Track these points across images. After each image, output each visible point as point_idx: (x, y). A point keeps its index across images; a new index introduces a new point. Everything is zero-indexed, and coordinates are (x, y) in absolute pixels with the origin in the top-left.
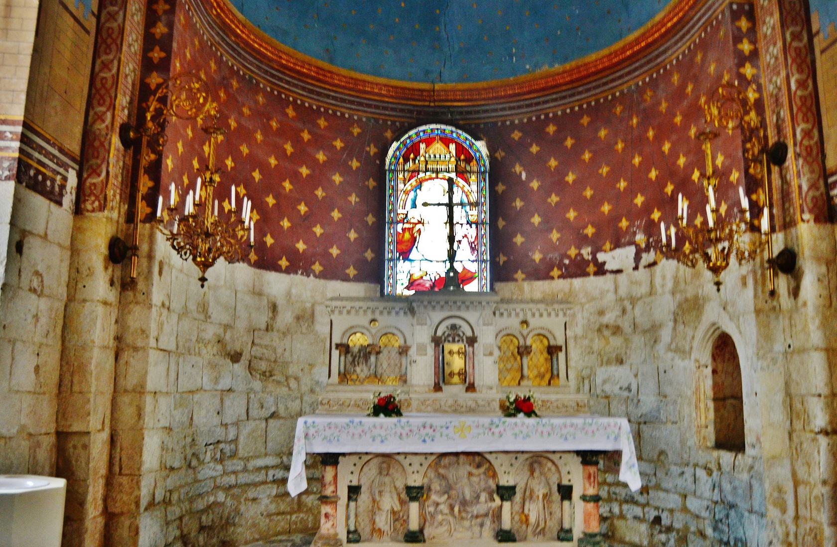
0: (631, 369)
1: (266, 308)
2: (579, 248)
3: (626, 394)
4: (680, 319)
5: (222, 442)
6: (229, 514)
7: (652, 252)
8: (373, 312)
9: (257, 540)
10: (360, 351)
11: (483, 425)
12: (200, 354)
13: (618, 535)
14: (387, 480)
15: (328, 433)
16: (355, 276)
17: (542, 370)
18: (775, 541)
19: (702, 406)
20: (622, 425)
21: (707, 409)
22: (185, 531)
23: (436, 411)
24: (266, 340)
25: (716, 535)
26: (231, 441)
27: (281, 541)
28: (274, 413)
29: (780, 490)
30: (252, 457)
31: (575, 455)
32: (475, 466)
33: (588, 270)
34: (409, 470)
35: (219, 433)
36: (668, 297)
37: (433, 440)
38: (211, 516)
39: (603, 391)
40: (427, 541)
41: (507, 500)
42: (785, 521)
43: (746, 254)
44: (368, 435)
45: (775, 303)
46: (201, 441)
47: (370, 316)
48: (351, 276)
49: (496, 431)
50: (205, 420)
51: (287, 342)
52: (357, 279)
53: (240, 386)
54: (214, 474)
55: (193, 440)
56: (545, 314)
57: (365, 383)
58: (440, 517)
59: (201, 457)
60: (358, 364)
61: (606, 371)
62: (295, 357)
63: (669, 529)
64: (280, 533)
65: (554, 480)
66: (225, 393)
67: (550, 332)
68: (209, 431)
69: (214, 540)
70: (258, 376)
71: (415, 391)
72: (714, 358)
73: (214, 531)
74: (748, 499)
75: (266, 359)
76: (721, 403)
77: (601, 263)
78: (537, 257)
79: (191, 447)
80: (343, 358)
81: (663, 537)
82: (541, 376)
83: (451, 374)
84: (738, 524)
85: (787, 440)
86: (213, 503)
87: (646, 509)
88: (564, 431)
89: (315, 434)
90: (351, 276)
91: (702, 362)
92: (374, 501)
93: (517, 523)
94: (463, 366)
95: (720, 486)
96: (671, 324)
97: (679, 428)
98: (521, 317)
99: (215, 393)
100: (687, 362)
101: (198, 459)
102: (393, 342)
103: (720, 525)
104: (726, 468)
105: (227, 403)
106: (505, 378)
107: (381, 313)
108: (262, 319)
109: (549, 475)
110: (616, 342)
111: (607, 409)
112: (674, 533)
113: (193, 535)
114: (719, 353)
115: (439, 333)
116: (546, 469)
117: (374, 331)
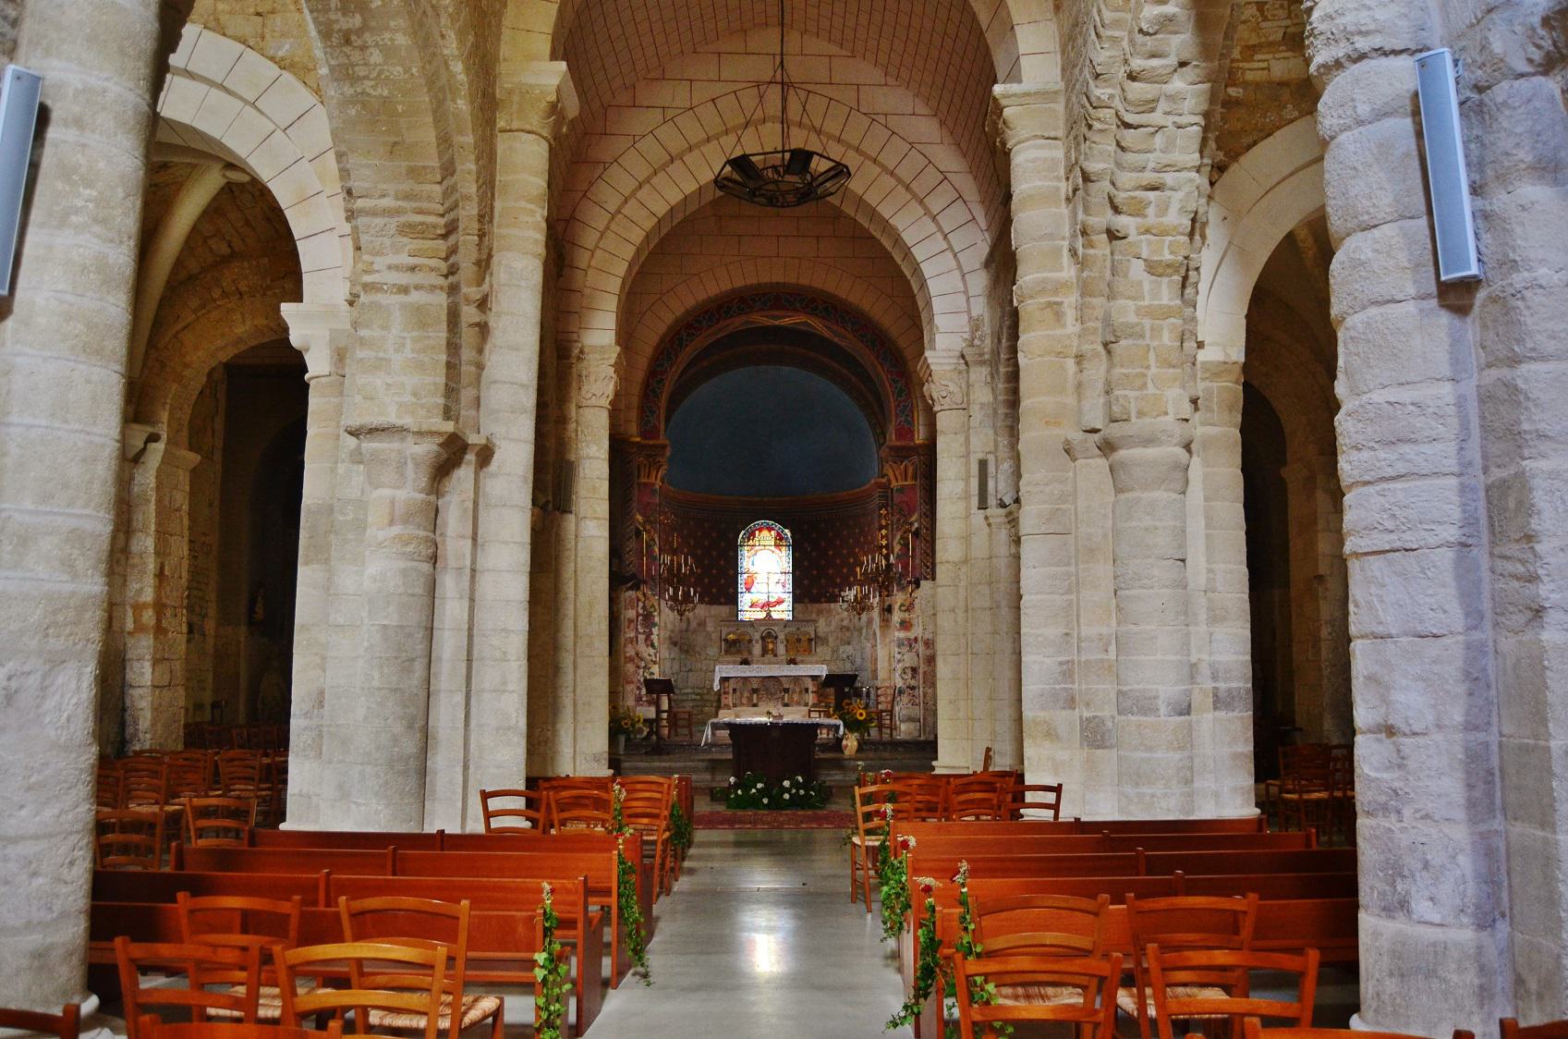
110: (848, 634)
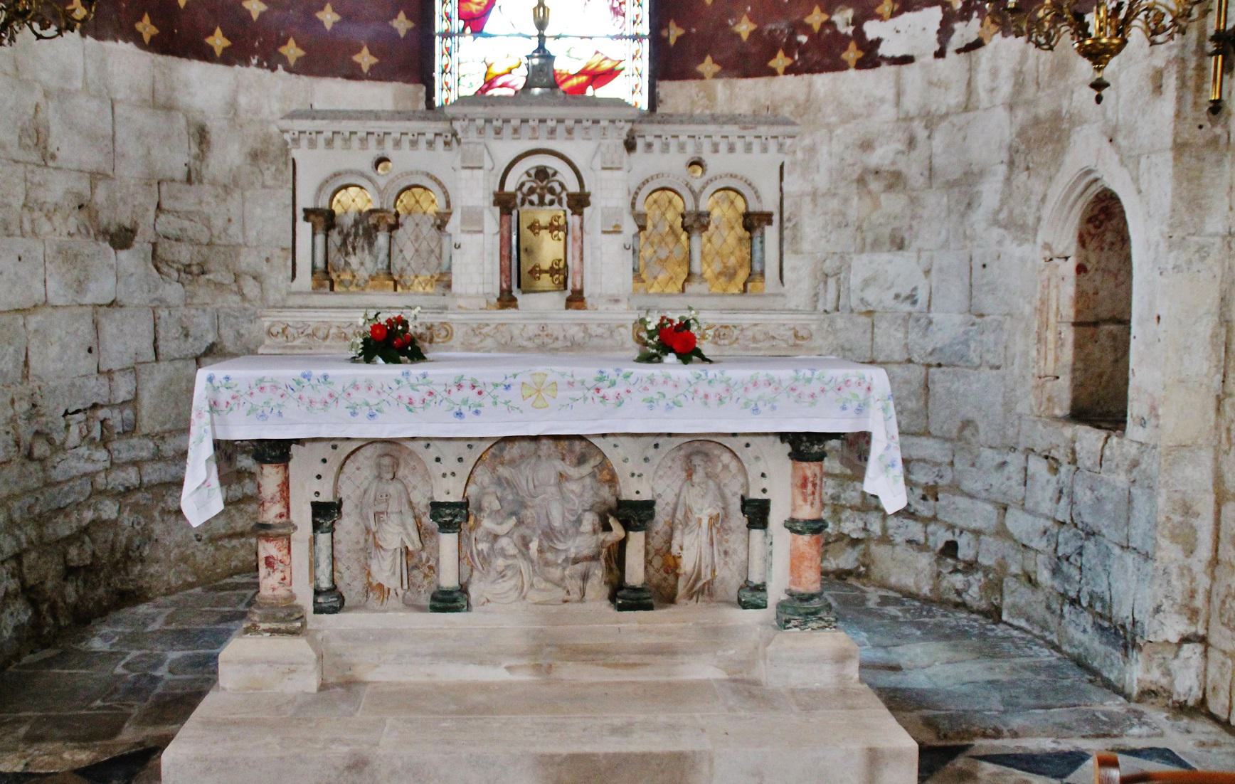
0: (919, 258)
1: (185, 137)
2: (829, 9)
3: (906, 307)
4: (1019, 159)
5: (102, 406)
6: (130, 540)
7: (975, 21)
8: (380, 142)
9: (192, 586)
10: (356, 224)
11: (583, 383)
12: (35, 233)
13: (876, 573)
14: (393, 489)
15: (259, 399)
16: (372, 68)
17: (732, 261)
18: (1166, 606)
19: (1050, 336)
20: (875, 382)
21: (1060, 343)
22: (31, 579)
23: (503, 347)
24: (188, 200)
25: (1056, 583)
26: (124, 402)
27: (237, 586)
28: (213, 345)
29: (1187, 510)
30: (170, 432)
31: (778, 440)
32: (575, 461)
33: (844, 56)
34: (437, 469)
35: (96, 389)
36: (1001, 114)
37: (477, 412)
38: (88, 548)
39: (862, 300)
40: (474, 608)
41: (636, 529)
42: (1190, 570)
43: (1167, 20)
44: (343, 403)
45: (1218, 130)
46: (53, 409)
47: (373, 152)
48: (365, 69)
49: (610, 392)
50: (60, 366)
51: (234, 204)
52: (377, 74)
53: (137, 296)
54: (89, 467)
55: (34, 406)
56: (739, 145)
57: (368, 290)
58: (500, 563)
59: (58, 438)
60: (354, 249)
61: (871, 262)
62: (252, 234)
63: (971, 567)
64: (238, 572)
65: (734, 491)
66: (101, 310)
67: (407, 174)
68: (73, 385)
69: (101, 591)
70: (175, 275)
71: (460, 307)
72: (1082, 242)
73: (97, 575)
74: (1123, 521)
75: (191, 240)
76: (1089, 331)
77: (872, 41)
78: (744, 28)
79: (29, 419)
80: (320, 238)
81: (958, 580)
82: (730, 274)
83: (535, 272)
84: (1099, 569)
85: (1212, 414)
86: (93, 521)
87: (932, 528)
88: (753, 394)
89: (232, 402)
90: (365, 69)
91: (1059, 249)
92: (368, 531)
93: (657, 571)
94: (561, 256)
95: (1071, 494)
96: (1002, 170)
97: (1004, 378)
98: (690, 153)
99: (80, 310)
100: (1027, 248)
101: (50, 441)
102: (425, 205)
103: (1065, 566)
104: (1086, 461)
105: (109, 328)
106: (655, 278)
107: (397, 144)
108: (176, 159)
109: (725, 478)
110: (893, 203)
111: (869, 336)
112: (980, 575)
113: (49, 584)
114: (1093, 231)
115: (510, 187)
116: (720, 466)
117: (382, 182)
